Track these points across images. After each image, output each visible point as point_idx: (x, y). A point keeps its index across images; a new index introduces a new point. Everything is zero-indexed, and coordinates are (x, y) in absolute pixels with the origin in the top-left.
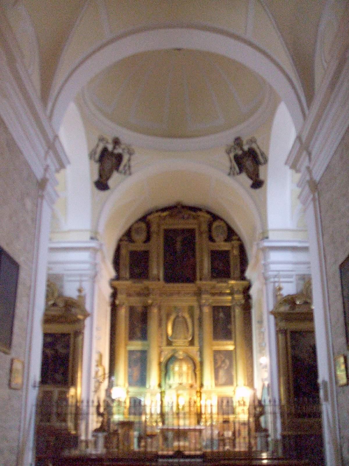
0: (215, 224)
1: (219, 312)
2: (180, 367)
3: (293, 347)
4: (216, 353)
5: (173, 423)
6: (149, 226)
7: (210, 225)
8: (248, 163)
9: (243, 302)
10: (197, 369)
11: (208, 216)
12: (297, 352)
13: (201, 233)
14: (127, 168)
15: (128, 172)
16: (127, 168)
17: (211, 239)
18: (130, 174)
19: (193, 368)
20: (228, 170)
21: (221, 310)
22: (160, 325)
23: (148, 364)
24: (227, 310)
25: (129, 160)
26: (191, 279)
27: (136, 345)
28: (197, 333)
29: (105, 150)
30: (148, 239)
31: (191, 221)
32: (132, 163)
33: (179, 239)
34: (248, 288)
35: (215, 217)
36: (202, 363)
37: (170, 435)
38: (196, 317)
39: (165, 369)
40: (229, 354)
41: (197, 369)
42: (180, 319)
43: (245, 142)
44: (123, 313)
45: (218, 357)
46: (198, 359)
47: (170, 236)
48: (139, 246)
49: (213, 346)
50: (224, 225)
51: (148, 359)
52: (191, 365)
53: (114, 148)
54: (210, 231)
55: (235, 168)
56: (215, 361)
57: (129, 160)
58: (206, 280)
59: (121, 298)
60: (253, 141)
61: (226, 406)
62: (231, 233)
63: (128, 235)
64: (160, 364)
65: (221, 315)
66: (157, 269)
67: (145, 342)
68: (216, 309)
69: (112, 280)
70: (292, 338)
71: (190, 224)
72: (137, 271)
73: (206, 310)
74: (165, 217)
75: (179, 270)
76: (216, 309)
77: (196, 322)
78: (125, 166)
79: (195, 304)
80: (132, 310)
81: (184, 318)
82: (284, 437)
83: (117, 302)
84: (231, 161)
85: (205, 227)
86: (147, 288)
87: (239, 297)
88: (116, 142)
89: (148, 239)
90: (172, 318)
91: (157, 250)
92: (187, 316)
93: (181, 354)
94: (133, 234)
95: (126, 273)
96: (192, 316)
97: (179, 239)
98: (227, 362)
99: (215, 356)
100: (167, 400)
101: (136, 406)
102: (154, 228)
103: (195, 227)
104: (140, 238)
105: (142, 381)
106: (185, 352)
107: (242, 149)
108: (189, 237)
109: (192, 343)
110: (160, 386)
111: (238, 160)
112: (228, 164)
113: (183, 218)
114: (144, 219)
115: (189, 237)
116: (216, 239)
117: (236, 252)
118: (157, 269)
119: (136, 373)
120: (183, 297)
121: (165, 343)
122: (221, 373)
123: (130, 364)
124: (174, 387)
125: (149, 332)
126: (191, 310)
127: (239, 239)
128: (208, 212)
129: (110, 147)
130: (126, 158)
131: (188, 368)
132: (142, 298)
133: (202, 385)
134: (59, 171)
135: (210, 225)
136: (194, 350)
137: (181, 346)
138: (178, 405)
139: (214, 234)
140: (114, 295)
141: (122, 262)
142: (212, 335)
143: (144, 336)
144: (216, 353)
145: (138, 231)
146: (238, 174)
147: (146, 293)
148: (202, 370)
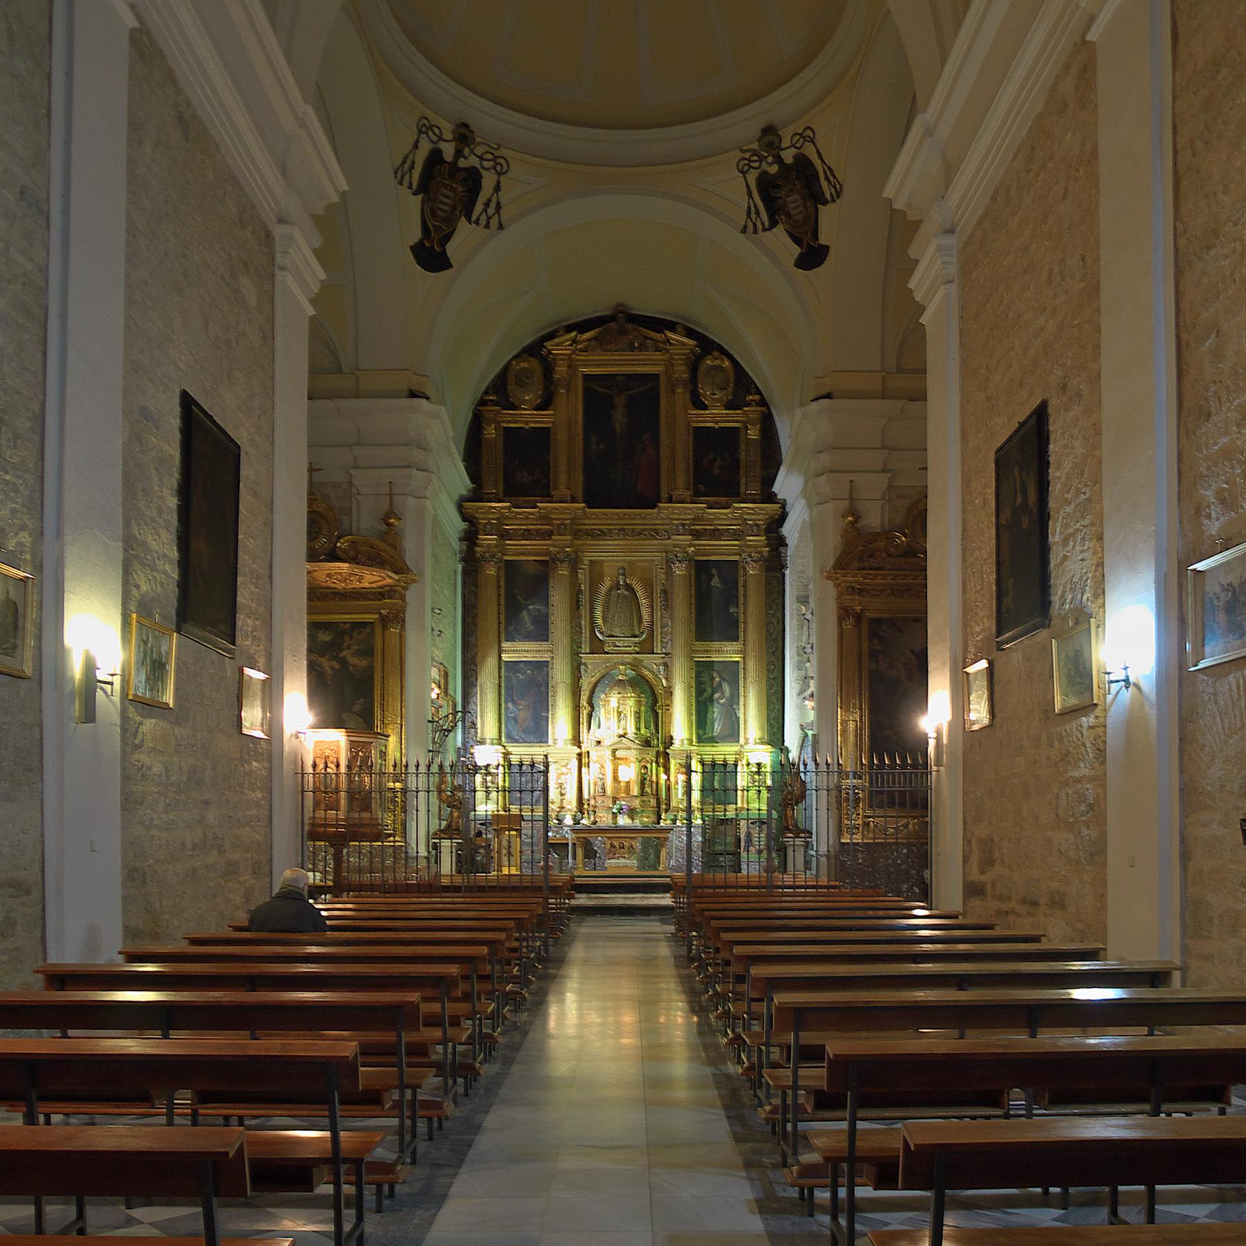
6: (548, 366)
7: (694, 368)
8: (794, 201)
14: (491, 211)
15: (494, 222)
16: (491, 211)
18: (501, 227)
20: (741, 220)
25: (497, 188)
29: (435, 157)
32: (504, 197)
33: (620, 401)
35: (707, 345)
37: (598, 842)
38: (658, 588)
43: (786, 142)
48: (527, 417)
53: (459, 154)
54: (694, 380)
55: (758, 213)
57: (497, 188)
60: (807, 135)
65: (716, 582)
70: (874, 634)
71: (645, 363)
75: (621, 483)
78: (487, 204)
84: (750, 194)
85: (682, 372)
88: (464, 135)
91: (565, 419)
94: (511, 387)
97: (620, 401)
99: (698, 675)
101: (529, 781)
102: (561, 371)
107: (779, 160)
110: (577, 741)
111: (767, 187)
112: (744, 202)
114: (535, 350)
115: (644, 394)
127: (763, 403)
129: (448, 151)
130: (488, 180)
139: (706, 391)
145: (522, 385)
146: (764, 230)
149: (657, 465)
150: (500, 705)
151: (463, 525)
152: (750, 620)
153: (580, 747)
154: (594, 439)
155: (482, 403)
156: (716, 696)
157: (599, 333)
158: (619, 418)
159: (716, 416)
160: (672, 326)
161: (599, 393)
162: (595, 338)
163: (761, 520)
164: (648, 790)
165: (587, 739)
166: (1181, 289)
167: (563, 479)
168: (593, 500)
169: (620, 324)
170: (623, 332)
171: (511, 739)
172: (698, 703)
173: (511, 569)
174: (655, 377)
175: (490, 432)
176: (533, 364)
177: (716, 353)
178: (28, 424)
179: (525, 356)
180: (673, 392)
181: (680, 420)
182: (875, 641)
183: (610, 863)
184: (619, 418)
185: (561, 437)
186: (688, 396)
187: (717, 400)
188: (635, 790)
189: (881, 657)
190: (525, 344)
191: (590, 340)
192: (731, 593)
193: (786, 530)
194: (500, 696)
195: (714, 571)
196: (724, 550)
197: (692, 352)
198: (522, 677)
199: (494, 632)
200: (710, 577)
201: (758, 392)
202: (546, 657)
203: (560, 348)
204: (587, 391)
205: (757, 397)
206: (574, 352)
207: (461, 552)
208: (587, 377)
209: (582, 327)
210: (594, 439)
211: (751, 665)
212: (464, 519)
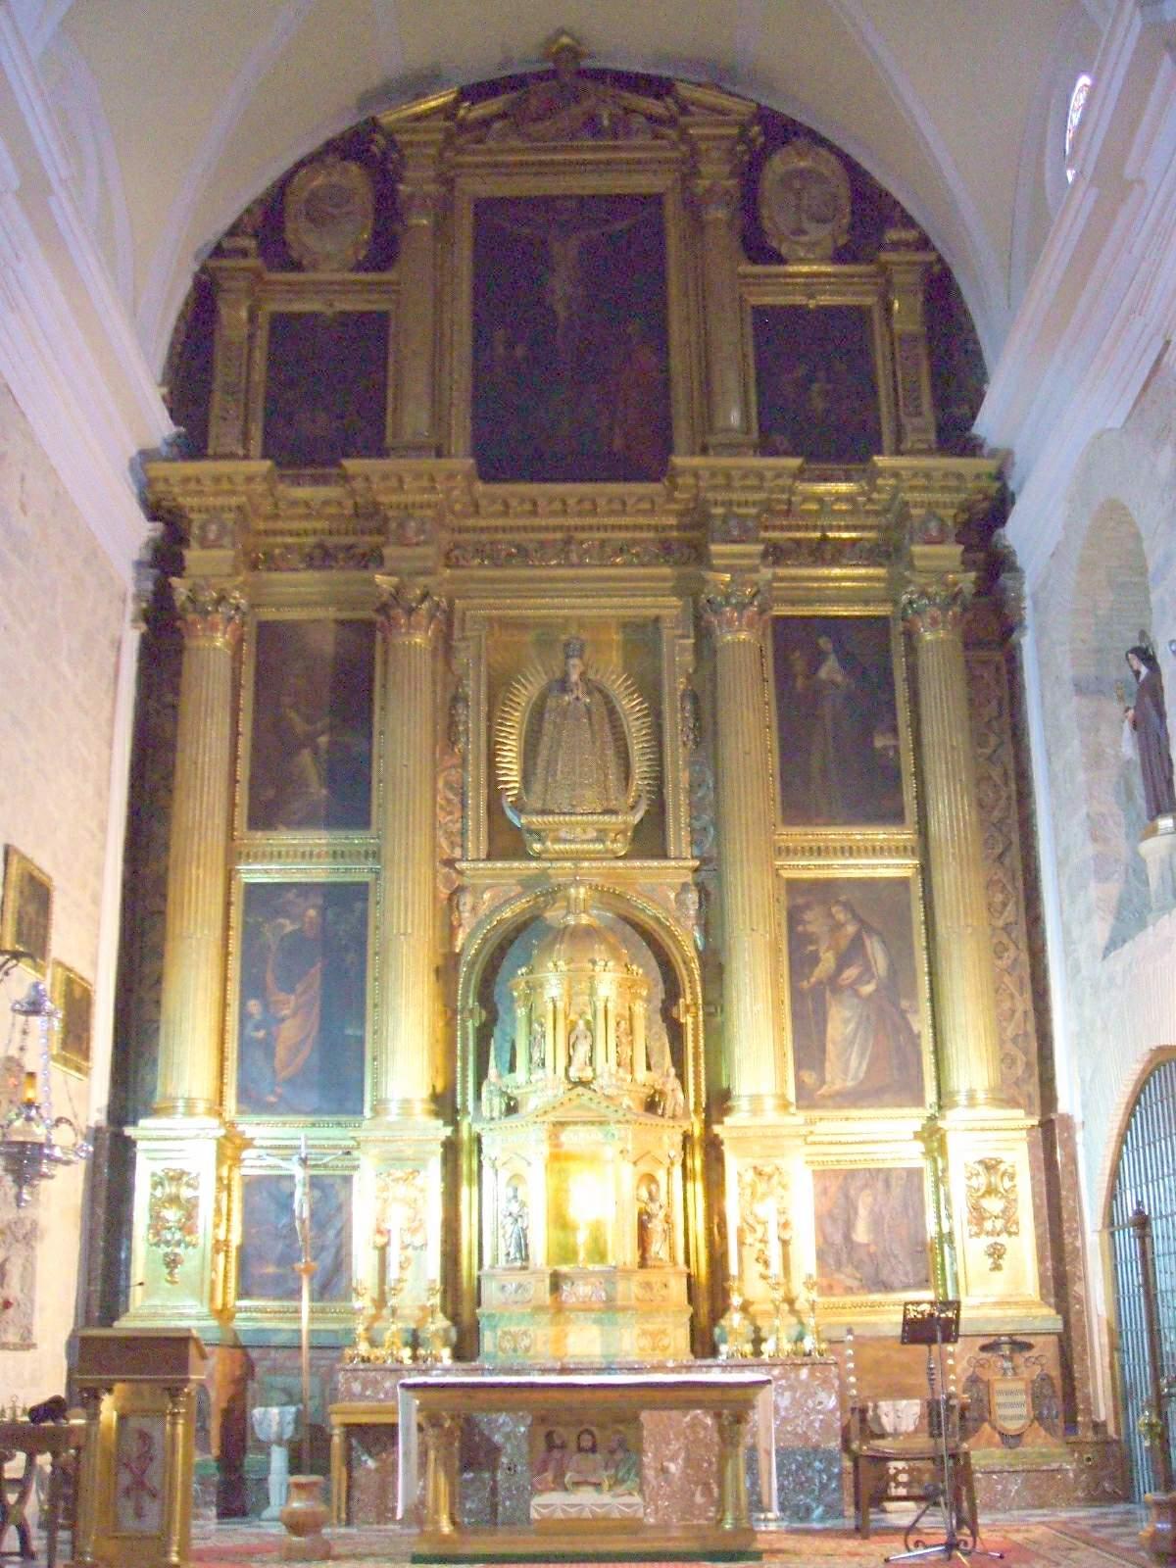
0: (778, 165)
2: (580, 983)
4: (803, 901)
5: (532, 1344)
7: (750, 172)
9: (968, 581)
10: (685, 996)
17: (758, 248)
19: (660, 993)
21: (824, 643)
22: (449, 733)
23: (371, 985)
24: (869, 650)
26: (642, 457)
27: (294, 859)
28: (679, 776)
30: (383, 251)
31: (640, 145)
33: (566, 252)
34: (997, 508)
35: (780, 130)
36: (714, 967)
37: (509, 1429)
38: (676, 686)
39: (481, 997)
40: (882, 911)
41: (685, 996)
42: (578, 697)
44: (214, 647)
45: (814, 922)
46: (687, 940)
47: (508, 241)
48: (329, 280)
49: (779, 856)
50: (829, 166)
51: (373, 943)
52: (644, 971)
54: (749, 202)
56: (800, 955)
58: (733, 448)
59: (206, 562)
61: (879, 1233)
62: (870, 215)
63: (268, 228)
64: (446, 970)
65: (830, 669)
66: (431, 378)
67: (357, 839)
68: (794, 639)
69: (146, 456)
71: (634, 170)
72: (317, 424)
73: (739, 636)
74: (485, 123)
75: (573, 394)
76: (794, 639)
77: (677, 721)
79: (670, 607)
80: (271, 646)
81: (594, 688)
85: (716, 173)
86: (370, 516)
87: (941, 559)
89: (383, 251)
90: (525, 694)
92: (617, 685)
93: (580, 908)
96: (650, 690)
97: (566, 252)
98: (878, 954)
99: (794, 917)
100: (490, 1209)
101: (292, 1240)
102: (417, 181)
105: (337, 1079)
106: (608, 897)
108: (627, 246)
109: (649, 839)
110: (445, 1105)
113: (592, 124)
114: (357, 144)
115: (627, 246)
117: (906, 312)
119: (295, 1029)
120: (588, 578)
121: (477, 842)
122: (841, 1021)
123: (254, 977)
124: (532, 1104)
125: (378, 768)
126: (642, 636)
127: (924, 243)
131: (628, 987)
132: (336, 577)
133: (718, 1102)
134: (144, 627)
135: (750, 172)
136: (663, 886)
137: (582, 846)
138: (561, 1222)
139: (776, 217)
140: (165, 558)
141: (224, 373)
142: (775, 788)
143: (350, 800)
144: (803, 901)
145: (318, 216)
147: (358, 543)
148: (715, 1004)
149: (663, 388)
150: (224, 1005)
152: (931, 733)
153: (455, 1124)
155: (218, 251)
156: (850, 973)
158: (562, 288)
159: (810, 277)
161: (508, 241)
163: (948, 504)
164: (658, 1248)
165: (481, 1119)
168: (496, 463)
169: (560, 87)
171: (251, 1099)
172: (797, 995)
174: (657, 200)
175: (233, 315)
176: (353, 176)
183: (549, 1503)
184: (562, 288)
187: (812, 246)
188: (623, 1251)
190: (327, 134)
193: (1015, 533)
194: (225, 979)
195: (824, 643)
196: (845, 587)
199: (216, 838)
200: (816, 660)
201: (909, 222)
202: (359, 873)
205: (910, 235)
208: (484, 207)
210: (500, 334)
211: (949, 879)
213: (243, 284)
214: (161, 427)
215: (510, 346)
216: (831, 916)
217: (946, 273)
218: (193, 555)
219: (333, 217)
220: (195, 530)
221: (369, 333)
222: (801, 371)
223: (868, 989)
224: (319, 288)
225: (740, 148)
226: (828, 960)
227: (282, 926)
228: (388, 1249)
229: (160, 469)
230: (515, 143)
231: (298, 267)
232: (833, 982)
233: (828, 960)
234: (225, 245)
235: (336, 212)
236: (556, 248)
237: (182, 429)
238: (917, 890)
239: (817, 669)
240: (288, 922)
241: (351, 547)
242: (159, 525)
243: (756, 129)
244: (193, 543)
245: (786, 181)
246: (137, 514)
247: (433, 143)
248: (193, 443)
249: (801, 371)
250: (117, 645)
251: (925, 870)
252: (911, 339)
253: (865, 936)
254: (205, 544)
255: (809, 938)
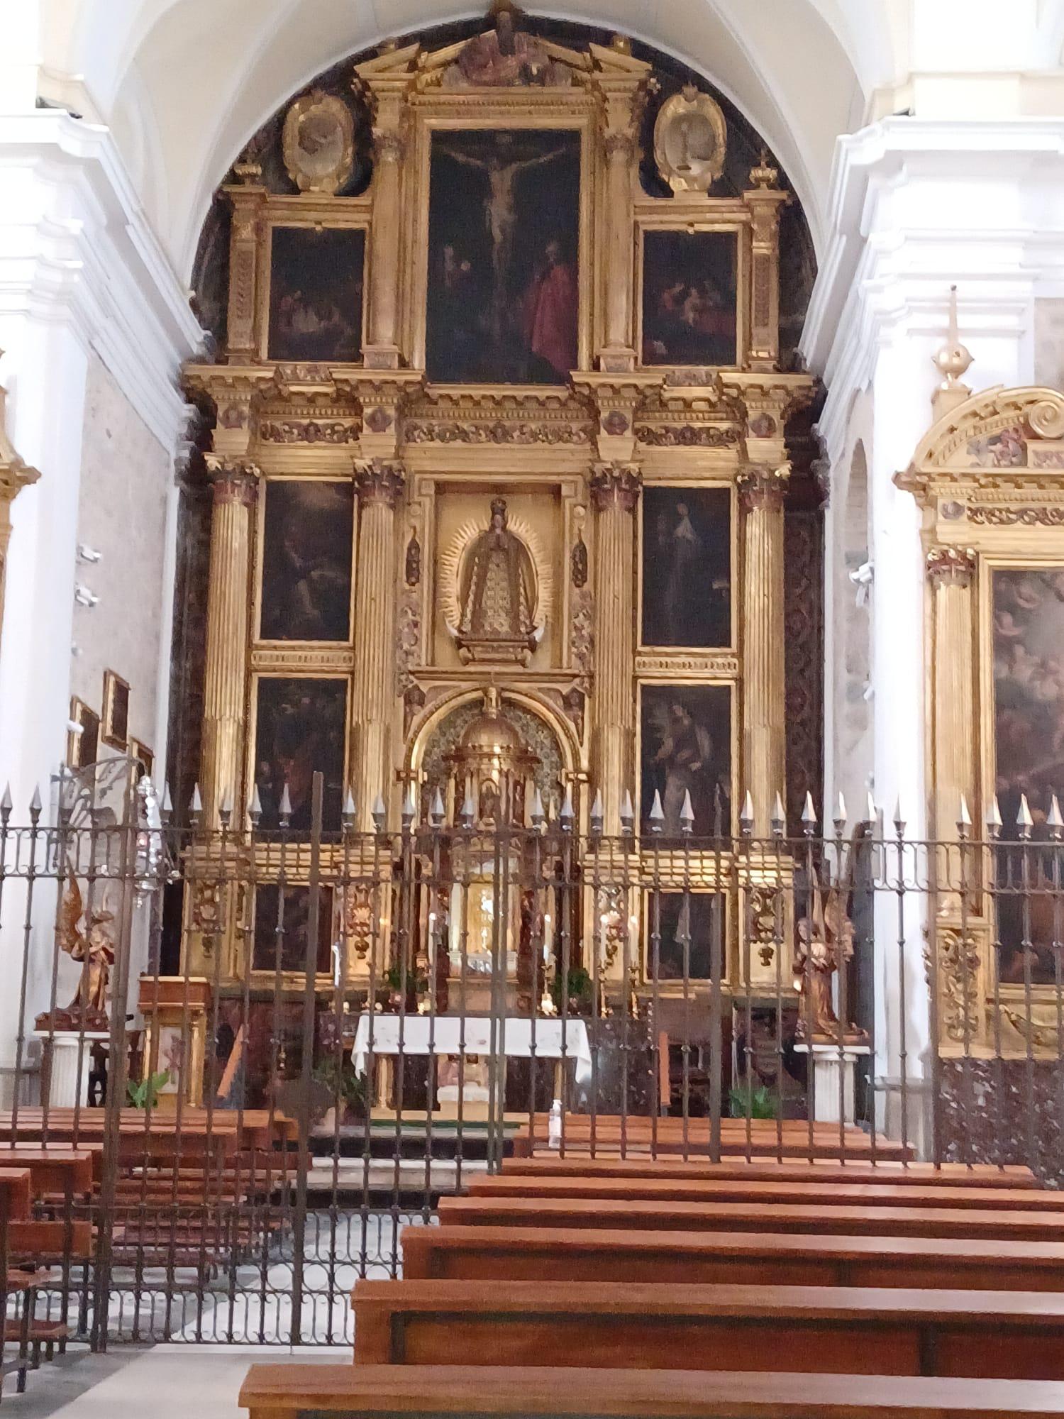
0: (676, 106)
1: (678, 519)
3: (1003, 647)
6: (363, 110)
11: (641, 68)
12: (1024, 673)
13: (604, 149)
17: (655, 185)
21: (682, 509)
30: (360, 181)
33: (502, 180)
35: (672, 75)
44: (237, 526)
47: (459, 169)
48: (320, 205)
50: (713, 112)
54: (646, 138)
59: (231, 443)
62: (745, 154)
63: (269, 147)
65: (684, 530)
66: (396, 331)
70: (1002, 604)
72: (308, 324)
75: (501, 316)
82: (940, 1066)
83: (212, 461)
85: (621, 123)
87: (768, 451)
89: (360, 181)
91: (398, 217)
94: (292, 151)
95: (250, 329)
97: (502, 180)
102: (386, 121)
103: (578, 122)
104: (324, 171)
108: (551, 165)
114: (340, 81)
115: (551, 165)
116: (677, 184)
118: (396, 331)
127: (782, 182)
128: (640, 50)
139: (667, 154)
140: (201, 435)
145: (309, 145)
151: (188, 411)
154: (449, 251)
155: (233, 178)
156: (685, 754)
157: (463, 51)
158: (499, 212)
159: (695, 208)
160: (607, 38)
161: (459, 169)
162: (456, 61)
166: (908, 1112)
167: (386, 329)
170: (506, 48)
173: (282, 501)
174: (573, 137)
175: (245, 233)
176: (333, 107)
177: (690, 90)
178: (782, 1050)
179: (319, 93)
180: (606, 162)
181: (613, 220)
182: (1007, 619)
184: (499, 212)
185: (383, 247)
186: (635, 171)
189: (1019, 651)
191: (445, 64)
192: (715, 556)
195: (682, 509)
197: (643, 84)
198: (290, 710)
201: (773, 163)
203: (385, 78)
204: (438, 161)
205: (772, 174)
206: (412, 85)
207: (178, 461)
208: (439, 137)
209: (432, 39)
210: (449, 251)
212: (189, 400)
213: (252, 206)
214: (195, 335)
215: (458, 260)
216: (672, 712)
217: (797, 204)
218: (219, 433)
219: (321, 145)
220: (220, 413)
221: (351, 247)
222: (678, 288)
223: (696, 766)
224: (307, 207)
225: (642, 93)
226: (669, 744)
227: (285, 709)
228: (554, 55)
229: (195, 370)
230: (464, 85)
231: (295, 190)
232: (671, 758)
233: (669, 744)
234: (239, 172)
235: (323, 141)
236: (495, 177)
237: (209, 333)
238: (20, 1101)
239: (675, 527)
240: (288, 706)
241: (332, 427)
242: (192, 406)
243: (653, 80)
244: (219, 424)
245: (678, 120)
246: (177, 398)
247: (398, 90)
248: (219, 348)
249: (678, 288)
250: (164, 501)
251: (740, 681)
252: (766, 259)
253: (697, 730)
254: (228, 426)
255: (658, 729)
